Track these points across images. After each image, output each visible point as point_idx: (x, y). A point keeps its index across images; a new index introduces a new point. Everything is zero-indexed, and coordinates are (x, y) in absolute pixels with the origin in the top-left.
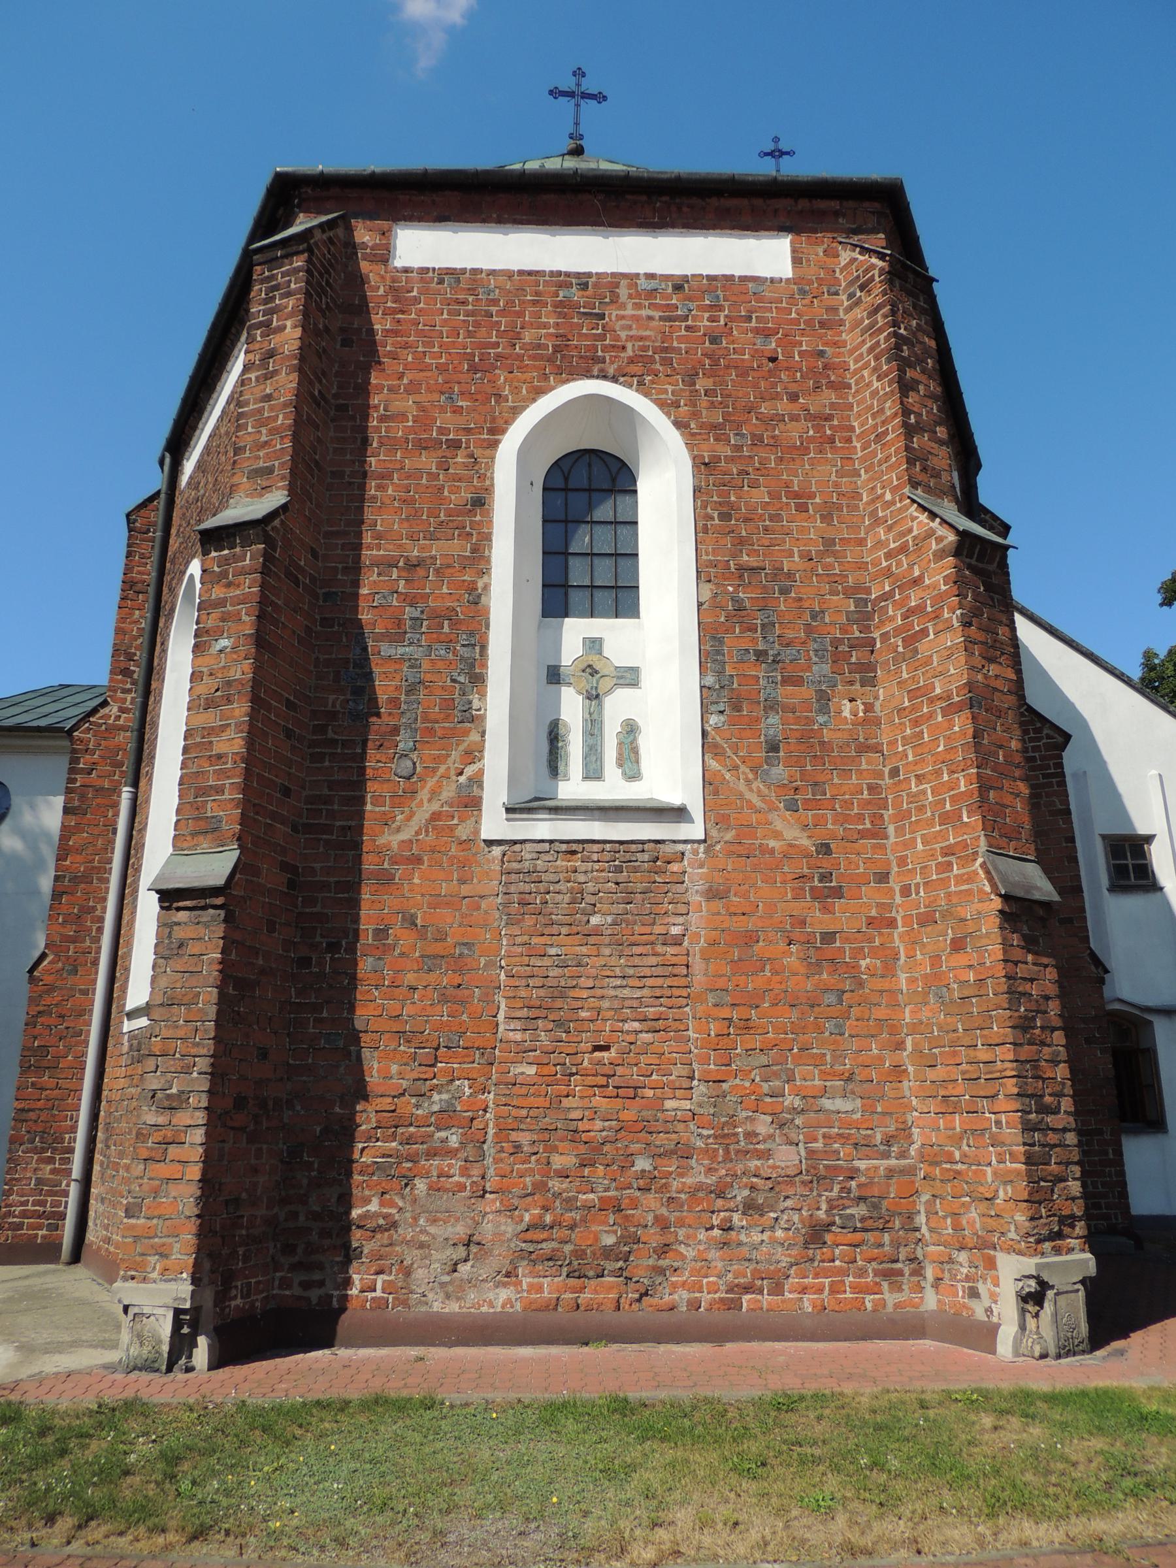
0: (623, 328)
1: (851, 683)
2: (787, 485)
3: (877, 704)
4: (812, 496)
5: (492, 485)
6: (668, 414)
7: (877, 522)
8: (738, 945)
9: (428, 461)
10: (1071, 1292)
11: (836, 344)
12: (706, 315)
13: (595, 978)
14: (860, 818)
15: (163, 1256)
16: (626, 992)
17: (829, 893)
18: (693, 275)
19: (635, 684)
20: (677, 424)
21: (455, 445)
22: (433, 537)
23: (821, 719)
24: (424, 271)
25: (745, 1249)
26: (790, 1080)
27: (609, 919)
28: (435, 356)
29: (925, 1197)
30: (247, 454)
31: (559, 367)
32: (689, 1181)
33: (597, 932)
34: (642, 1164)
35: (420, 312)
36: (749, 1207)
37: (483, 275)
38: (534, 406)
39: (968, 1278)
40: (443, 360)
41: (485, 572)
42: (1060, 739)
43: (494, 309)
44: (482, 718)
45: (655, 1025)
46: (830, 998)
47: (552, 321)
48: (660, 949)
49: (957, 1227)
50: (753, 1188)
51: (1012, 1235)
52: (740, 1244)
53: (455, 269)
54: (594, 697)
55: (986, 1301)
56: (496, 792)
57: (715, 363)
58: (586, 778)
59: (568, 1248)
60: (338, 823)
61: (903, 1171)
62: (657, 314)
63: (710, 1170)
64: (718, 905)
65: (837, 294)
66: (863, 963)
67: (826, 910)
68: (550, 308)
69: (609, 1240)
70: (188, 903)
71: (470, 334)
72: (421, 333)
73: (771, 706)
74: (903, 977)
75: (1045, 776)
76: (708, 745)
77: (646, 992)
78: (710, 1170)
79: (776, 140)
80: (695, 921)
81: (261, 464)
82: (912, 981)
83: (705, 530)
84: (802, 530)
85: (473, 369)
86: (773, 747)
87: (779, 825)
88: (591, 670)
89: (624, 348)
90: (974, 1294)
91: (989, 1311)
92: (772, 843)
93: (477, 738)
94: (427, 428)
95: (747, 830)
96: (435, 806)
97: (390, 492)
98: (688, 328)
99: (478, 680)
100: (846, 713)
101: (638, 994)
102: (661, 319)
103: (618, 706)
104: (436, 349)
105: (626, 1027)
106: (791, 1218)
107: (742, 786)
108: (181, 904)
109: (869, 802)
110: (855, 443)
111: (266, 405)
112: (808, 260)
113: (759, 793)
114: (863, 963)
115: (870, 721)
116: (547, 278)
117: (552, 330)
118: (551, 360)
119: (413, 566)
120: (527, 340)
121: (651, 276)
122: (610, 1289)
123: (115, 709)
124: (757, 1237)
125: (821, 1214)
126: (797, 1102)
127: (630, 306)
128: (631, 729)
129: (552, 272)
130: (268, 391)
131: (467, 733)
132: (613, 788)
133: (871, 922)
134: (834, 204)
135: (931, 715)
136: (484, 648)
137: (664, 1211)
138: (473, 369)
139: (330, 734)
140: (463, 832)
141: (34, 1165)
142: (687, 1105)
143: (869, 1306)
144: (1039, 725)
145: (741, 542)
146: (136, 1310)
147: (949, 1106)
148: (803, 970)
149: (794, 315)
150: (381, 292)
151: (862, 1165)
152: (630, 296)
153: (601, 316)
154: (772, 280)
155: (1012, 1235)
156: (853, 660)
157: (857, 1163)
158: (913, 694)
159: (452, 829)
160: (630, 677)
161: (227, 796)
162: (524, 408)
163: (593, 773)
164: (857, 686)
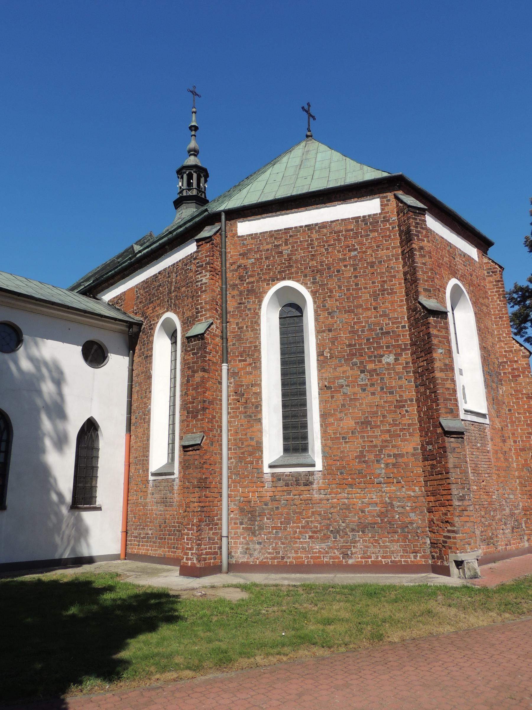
7: (501, 341)
15: (470, 544)
70: (455, 436)
108: (453, 436)
135: (523, 398)
141: (207, 532)
146: (467, 561)
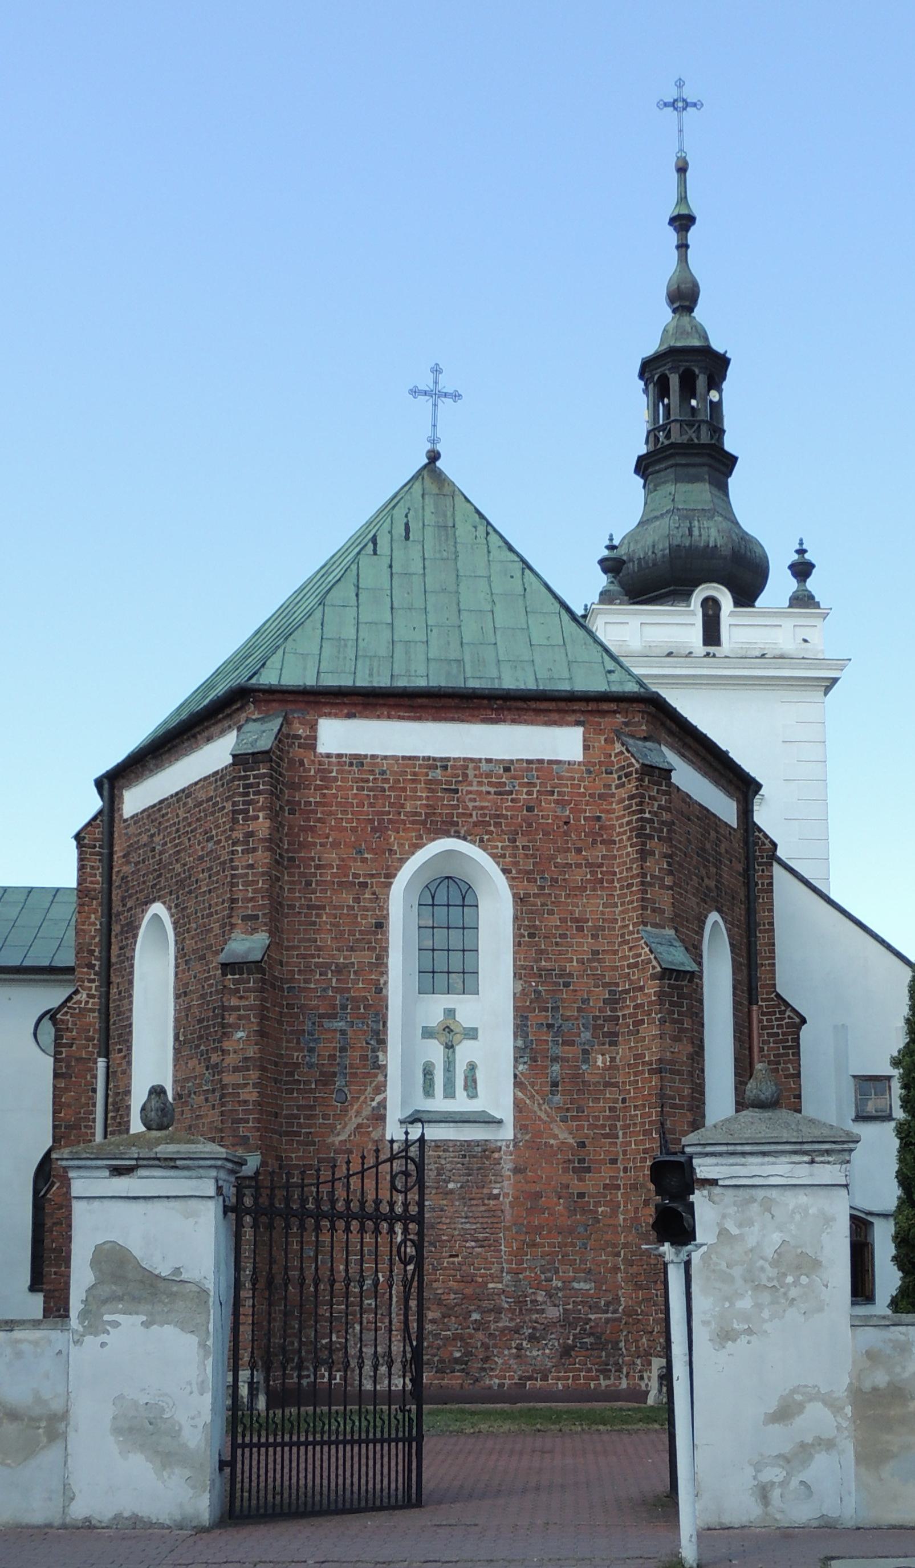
0: (471, 800)
1: (604, 1044)
2: (572, 913)
3: (618, 1058)
4: (587, 921)
5: (388, 914)
6: (498, 863)
7: (625, 942)
8: (530, 1200)
9: (347, 898)
10: (144, 1159)
11: (608, 812)
12: (525, 790)
13: (451, 1218)
14: (603, 1126)
16: (468, 1226)
17: (582, 1169)
18: (517, 760)
19: (475, 1038)
20: (505, 871)
21: (364, 885)
22: (352, 949)
23: (584, 1067)
24: (339, 756)
25: (529, 1359)
26: (557, 1272)
27: (459, 1185)
28: (349, 821)
29: (625, 1333)
30: (240, 904)
31: (429, 829)
32: (500, 1325)
33: (452, 1192)
34: (475, 1316)
35: (338, 788)
36: (532, 1338)
37: (379, 760)
38: (413, 857)
39: (640, 1371)
40: (354, 824)
41: (385, 973)
42: (797, 1020)
43: (386, 786)
44: (385, 1066)
45: (481, 1243)
46: (581, 1229)
47: (424, 795)
48: (486, 1202)
49: (637, 1347)
50: (534, 1328)
51: (659, 1349)
52: (527, 1356)
53: (360, 755)
54: (450, 1047)
55: (646, 1381)
56: (394, 1114)
57: (530, 825)
58: (445, 1097)
59: (436, 1359)
60: (303, 1131)
61: (615, 1320)
62: (492, 790)
63: (511, 1320)
64: (520, 1176)
65: (611, 773)
66: (600, 1210)
67: (581, 1179)
68: (423, 785)
69: (458, 1355)
71: (371, 805)
72: (339, 804)
73: (555, 1059)
74: (621, 1217)
75: (784, 1048)
76: (518, 1084)
77: (478, 1225)
78: (511, 1320)
79: (680, 84)
80: (505, 1187)
81: (250, 912)
82: (354, 1329)
83: (519, 944)
84: (580, 944)
85: (374, 830)
86: (555, 1084)
87: (556, 1131)
88: (448, 1029)
89: (471, 815)
90: (641, 1378)
91: (647, 1385)
92: (552, 1142)
93: (383, 1079)
94: (347, 875)
95: (538, 1134)
96: (359, 1120)
97: (324, 919)
98: (512, 800)
99: (382, 1042)
100: (599, 1063)
101: (474, 1227)
102: (496, 793)
103: (466, 1052)
104: (350, 816)
105: (468, 1245)
106: (553, 1342)
107: (536, 1108)
109: (609, 1117)
110: (616, 884)
111: (250, 871)
112: (594, 747)
113: (546, 1112)
114: (600, 1210)
115: (612, 1067)
116: (421, 762)
117: (424, 802)
118: (424, 823)
119: (339, 970)
120: (408, 809)
121: (489, 761)
122: (458, 1378)
123: (84, 996)
124: (535, 1353)
125: (570, 1342)
126: (560, 1284)
127: (475, 783)
128: (472, 1067)
129: (424, 757)
130: (250, 862)
131: (376, 1076)
132: (461, 1103)
133: (606, 1186)
134: (613, 706)
136: (385, 1024)
137: (487, 1340)
138: (374, 830)
139: (296, 1077)
140: (375, 1135)
142: (500, 1286)
143: (592, 1386)
144: (783, 1008)
145: (541, 952)
147: (638, 1287)
148: (566, 1214)
149: (582, 790)
150: (312, 773)
151: (592, 1317)
152: (475, 776)
153: (456, 791)
154: (569, 763)
155: (659, 1349)
156: (606, 1029)
157: (590, 1316)
158: (637, 1057)
159: (369, 1133)
160: (472, 1034)
161: (251, 1124)
162: (408, 859)
163: (450, 1093)
164: (607, 1046)
